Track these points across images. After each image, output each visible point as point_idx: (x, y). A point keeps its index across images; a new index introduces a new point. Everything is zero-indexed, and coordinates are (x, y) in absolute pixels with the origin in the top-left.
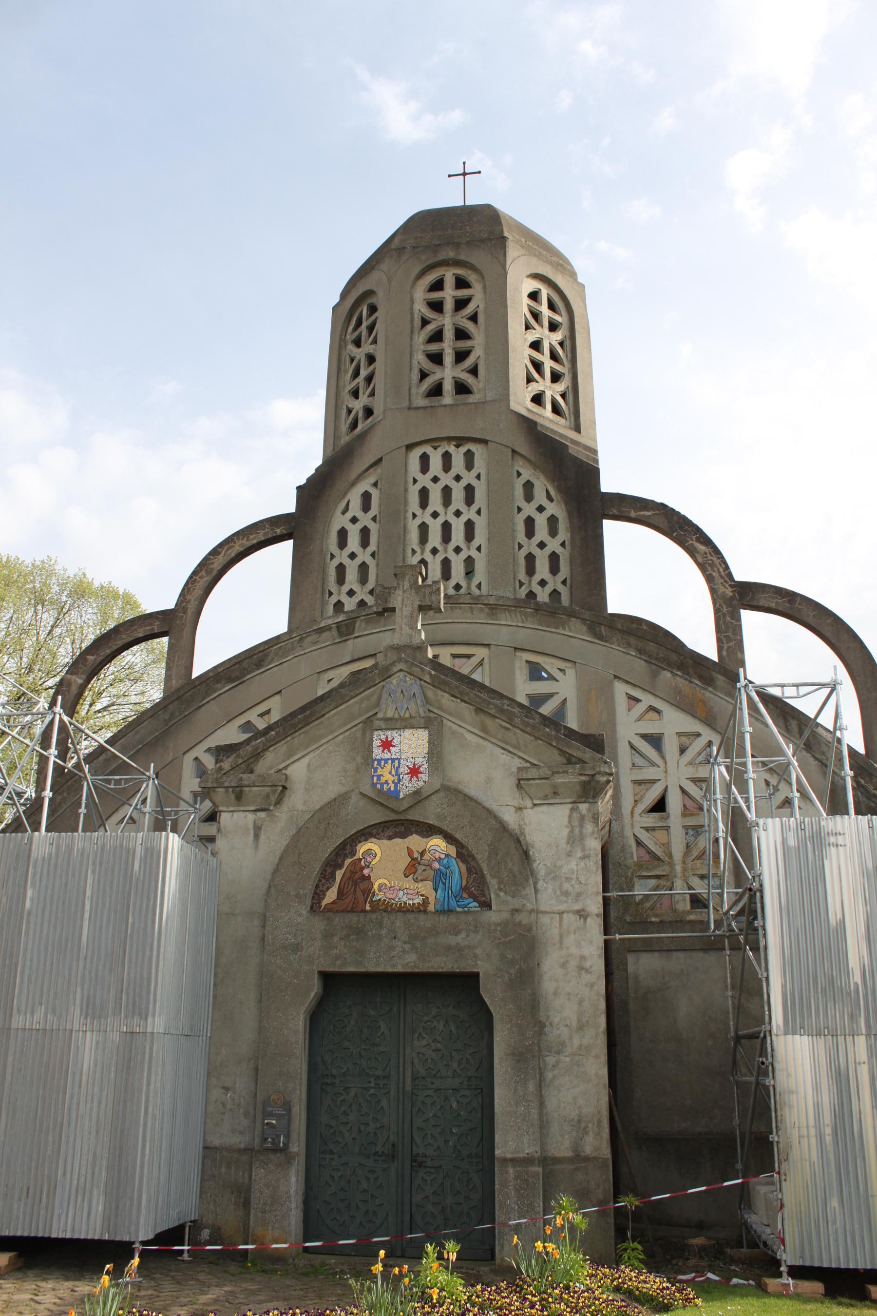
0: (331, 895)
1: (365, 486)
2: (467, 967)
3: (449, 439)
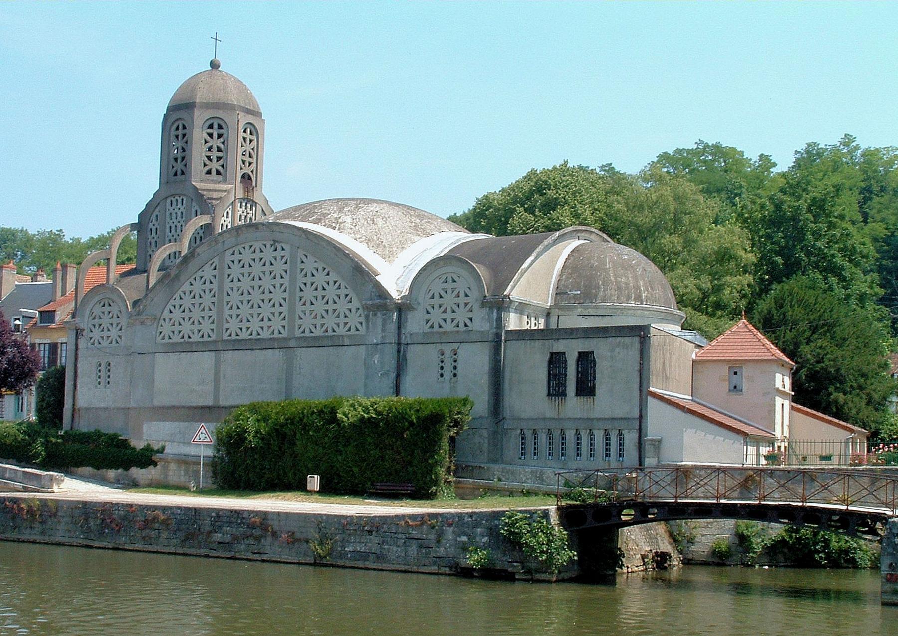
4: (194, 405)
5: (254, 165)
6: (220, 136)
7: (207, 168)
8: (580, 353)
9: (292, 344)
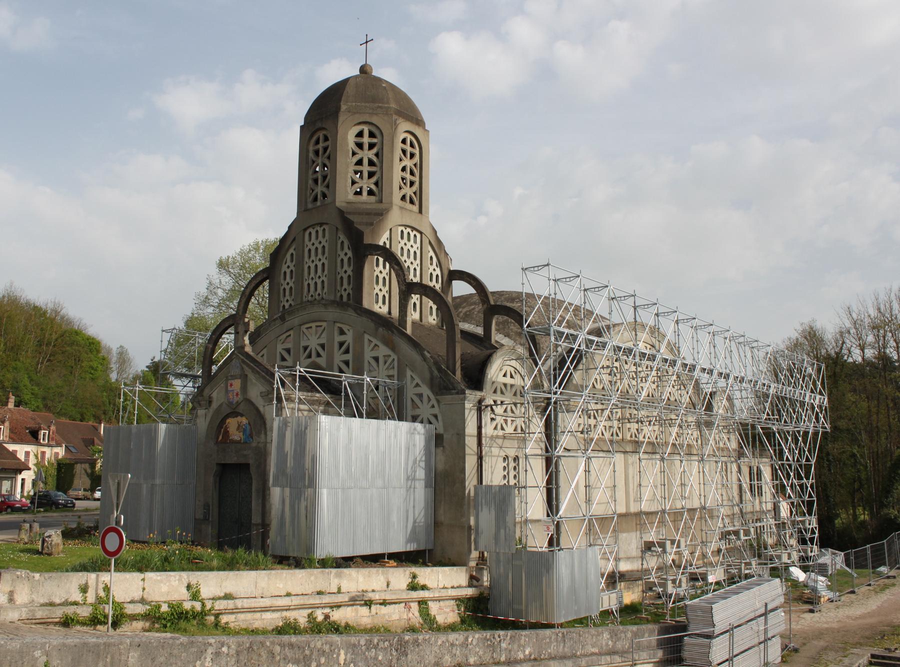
0: (220, 438)
1: (291, 251)
2: (242, 461)
3: (317, 224)
5: (417, 185)
6: (371, 146)
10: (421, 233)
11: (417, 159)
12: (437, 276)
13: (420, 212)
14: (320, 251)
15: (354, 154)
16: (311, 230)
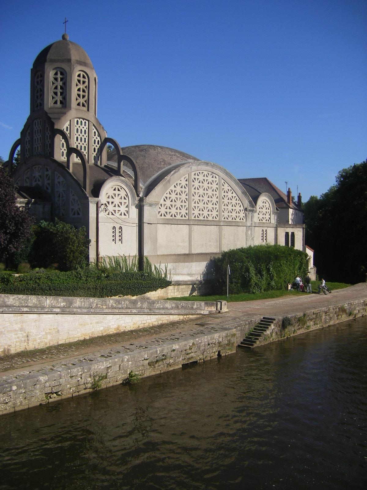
1: (29, 131)
4: (179, 253)
7: (54, 100)
8: (288, 232)
9: (222, 224)
10: (88, 121)
11: (87, 84)
12: (98, 141)
13: (88, 110)
14: (37, 132)
15: (53, 83)
16: (35, 121)
